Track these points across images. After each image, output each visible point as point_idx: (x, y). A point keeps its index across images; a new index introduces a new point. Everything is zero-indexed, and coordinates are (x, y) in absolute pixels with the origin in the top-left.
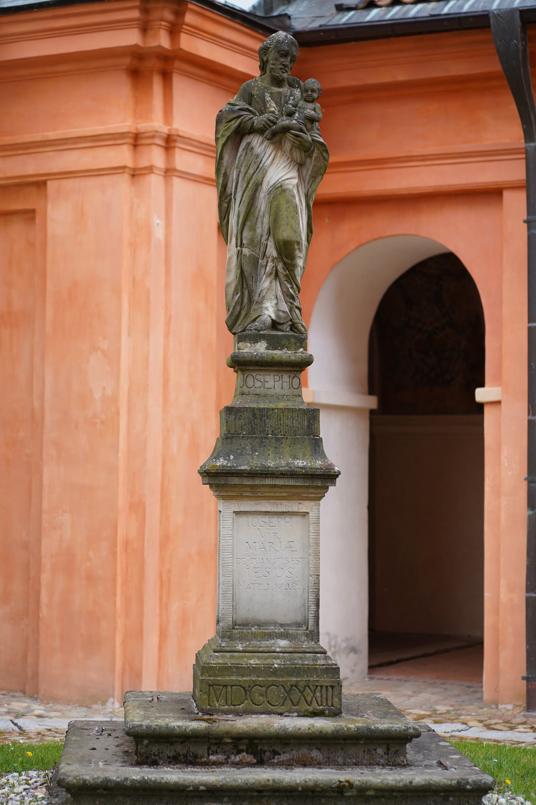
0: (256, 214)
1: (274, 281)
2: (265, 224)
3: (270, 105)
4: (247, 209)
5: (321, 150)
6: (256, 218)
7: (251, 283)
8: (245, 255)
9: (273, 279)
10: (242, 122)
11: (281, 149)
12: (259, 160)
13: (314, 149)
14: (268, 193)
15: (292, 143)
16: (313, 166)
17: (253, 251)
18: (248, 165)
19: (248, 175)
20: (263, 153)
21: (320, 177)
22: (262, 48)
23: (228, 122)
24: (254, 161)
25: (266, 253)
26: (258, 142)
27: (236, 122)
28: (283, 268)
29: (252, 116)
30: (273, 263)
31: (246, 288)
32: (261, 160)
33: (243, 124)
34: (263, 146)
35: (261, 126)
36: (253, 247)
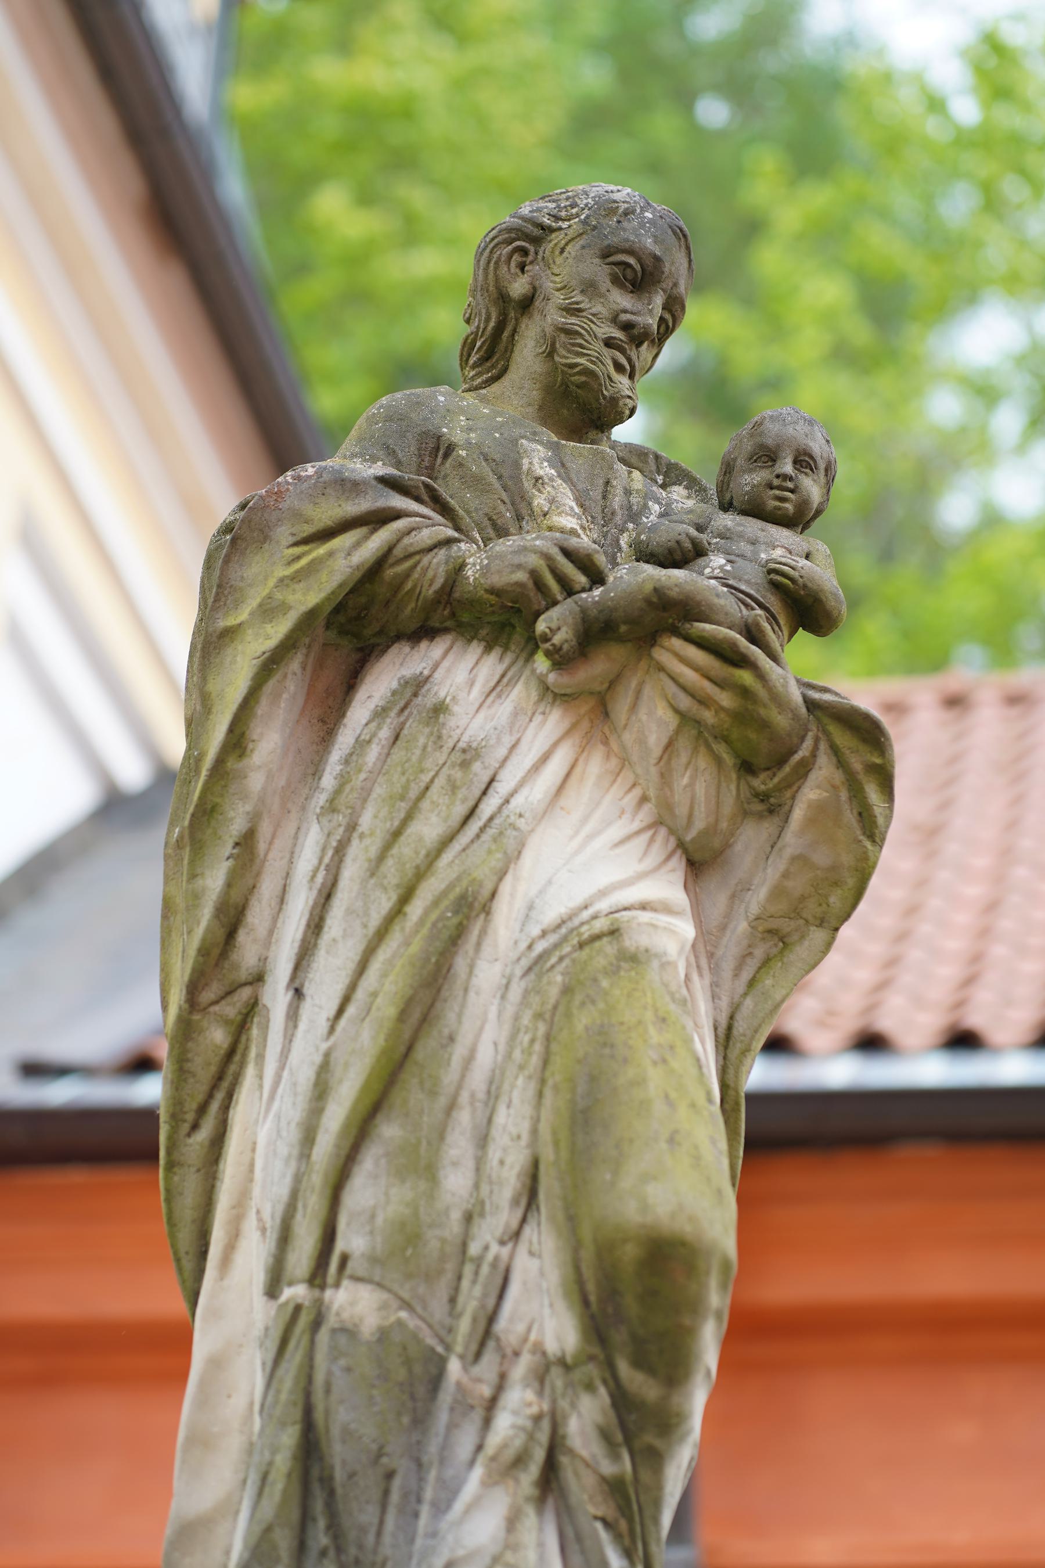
0: (449, 1078)
1: (530, 1511)
2: (500, 1139)
3: (552, 501)
4: (393, 1035)
5: (857, 766)
6: (443, 1101)
7: (368, 1515)
8: (348, 1332)
9: (528, 1499)
10: (398, 552)
11: (606, 742)
12: (480, 772)
13: (814, 755)
14: (525, 963)
15: (685, 702)
16: (794, 859)
17: (406, 1305)
18: (413, 794)
19: (408, 851)
20: (508, 741)
21: (818, 935)
22: (509, 230)
23: (305, 541)
24: (449, 779)
25: (502, 1324)
26: (472, 683)
27: (358, 545)
28: (605, 1435)
29: (451, 533)
30: (540, 1393)
31: (323, 1553)
32: (492, 781)
33: (393, 565)
34: (504, 709)
35: (521, 576)
36: (409, 1276)
